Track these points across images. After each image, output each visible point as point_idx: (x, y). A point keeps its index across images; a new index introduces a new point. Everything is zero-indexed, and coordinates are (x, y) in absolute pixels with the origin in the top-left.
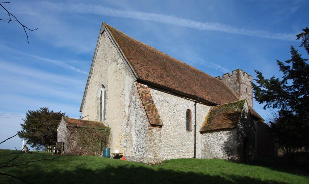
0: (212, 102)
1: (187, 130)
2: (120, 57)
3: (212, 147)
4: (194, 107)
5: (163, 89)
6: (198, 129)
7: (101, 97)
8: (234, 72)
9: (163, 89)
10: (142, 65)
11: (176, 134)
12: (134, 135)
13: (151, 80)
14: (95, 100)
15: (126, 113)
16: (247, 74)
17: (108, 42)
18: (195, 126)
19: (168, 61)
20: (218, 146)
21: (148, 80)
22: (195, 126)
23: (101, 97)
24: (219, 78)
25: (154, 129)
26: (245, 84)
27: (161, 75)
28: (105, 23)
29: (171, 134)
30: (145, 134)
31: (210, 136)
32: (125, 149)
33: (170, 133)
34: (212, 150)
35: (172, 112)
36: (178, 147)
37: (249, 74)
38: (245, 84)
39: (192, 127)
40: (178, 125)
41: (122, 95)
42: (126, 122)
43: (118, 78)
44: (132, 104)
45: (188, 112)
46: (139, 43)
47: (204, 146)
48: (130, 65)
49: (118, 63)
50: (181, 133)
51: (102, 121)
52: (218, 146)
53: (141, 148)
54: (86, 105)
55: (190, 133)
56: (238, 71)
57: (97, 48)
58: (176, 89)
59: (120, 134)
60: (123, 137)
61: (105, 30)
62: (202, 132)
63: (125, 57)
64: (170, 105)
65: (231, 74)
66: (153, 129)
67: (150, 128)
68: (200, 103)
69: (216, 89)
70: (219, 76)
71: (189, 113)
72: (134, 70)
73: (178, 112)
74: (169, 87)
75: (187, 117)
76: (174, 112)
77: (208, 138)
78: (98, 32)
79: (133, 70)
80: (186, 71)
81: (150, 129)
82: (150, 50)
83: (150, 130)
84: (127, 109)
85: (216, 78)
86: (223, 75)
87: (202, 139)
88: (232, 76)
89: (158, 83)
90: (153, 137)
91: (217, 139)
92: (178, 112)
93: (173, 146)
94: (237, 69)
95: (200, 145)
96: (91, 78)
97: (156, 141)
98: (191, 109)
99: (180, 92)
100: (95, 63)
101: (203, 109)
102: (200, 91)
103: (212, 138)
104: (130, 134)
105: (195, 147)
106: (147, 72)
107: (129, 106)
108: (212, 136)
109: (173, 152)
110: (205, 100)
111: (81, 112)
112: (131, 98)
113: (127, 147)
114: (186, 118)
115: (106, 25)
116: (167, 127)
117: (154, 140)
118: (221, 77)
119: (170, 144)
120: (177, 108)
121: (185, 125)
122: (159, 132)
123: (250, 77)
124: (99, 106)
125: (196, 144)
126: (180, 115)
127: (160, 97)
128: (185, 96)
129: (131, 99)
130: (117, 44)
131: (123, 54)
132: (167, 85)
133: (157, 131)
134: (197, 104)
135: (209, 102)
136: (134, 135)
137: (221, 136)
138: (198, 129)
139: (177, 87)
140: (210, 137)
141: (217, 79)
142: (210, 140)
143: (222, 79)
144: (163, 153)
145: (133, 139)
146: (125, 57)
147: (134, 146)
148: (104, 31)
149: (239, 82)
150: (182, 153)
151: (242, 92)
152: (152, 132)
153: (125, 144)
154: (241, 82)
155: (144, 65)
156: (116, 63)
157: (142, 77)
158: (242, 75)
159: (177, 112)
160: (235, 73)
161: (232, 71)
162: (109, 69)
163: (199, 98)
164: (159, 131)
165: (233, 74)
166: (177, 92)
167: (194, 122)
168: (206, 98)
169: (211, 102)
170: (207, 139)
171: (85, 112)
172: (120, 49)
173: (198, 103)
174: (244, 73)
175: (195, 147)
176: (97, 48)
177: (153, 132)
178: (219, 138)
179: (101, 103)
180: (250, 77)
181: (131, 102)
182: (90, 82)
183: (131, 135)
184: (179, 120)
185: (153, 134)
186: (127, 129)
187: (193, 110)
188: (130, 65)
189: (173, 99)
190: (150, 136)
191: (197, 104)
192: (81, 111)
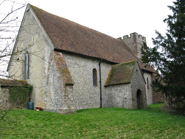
0: (113, 61)
18: (100, 81)
22: (100, 81)
25: (68, 88)
32: (46, 103)
39: (98, 83)
44: (51, 67)
45: (95, 70)
55: (97, 87)
64: (80, 66)
75: (93, 75)
84: (46, 71)
92: (86, 71)
97: (69, 96)
103: (113, 91)
107: (48, 69)
109: (83, 104)
120: (85, 69)
121: (92, 82)
137: (120, 89)
138: (103, 84)
150: (90, 104)
153: (46, 99)
164: (71, 88)
175: (101, 99)
178: (119, 91)
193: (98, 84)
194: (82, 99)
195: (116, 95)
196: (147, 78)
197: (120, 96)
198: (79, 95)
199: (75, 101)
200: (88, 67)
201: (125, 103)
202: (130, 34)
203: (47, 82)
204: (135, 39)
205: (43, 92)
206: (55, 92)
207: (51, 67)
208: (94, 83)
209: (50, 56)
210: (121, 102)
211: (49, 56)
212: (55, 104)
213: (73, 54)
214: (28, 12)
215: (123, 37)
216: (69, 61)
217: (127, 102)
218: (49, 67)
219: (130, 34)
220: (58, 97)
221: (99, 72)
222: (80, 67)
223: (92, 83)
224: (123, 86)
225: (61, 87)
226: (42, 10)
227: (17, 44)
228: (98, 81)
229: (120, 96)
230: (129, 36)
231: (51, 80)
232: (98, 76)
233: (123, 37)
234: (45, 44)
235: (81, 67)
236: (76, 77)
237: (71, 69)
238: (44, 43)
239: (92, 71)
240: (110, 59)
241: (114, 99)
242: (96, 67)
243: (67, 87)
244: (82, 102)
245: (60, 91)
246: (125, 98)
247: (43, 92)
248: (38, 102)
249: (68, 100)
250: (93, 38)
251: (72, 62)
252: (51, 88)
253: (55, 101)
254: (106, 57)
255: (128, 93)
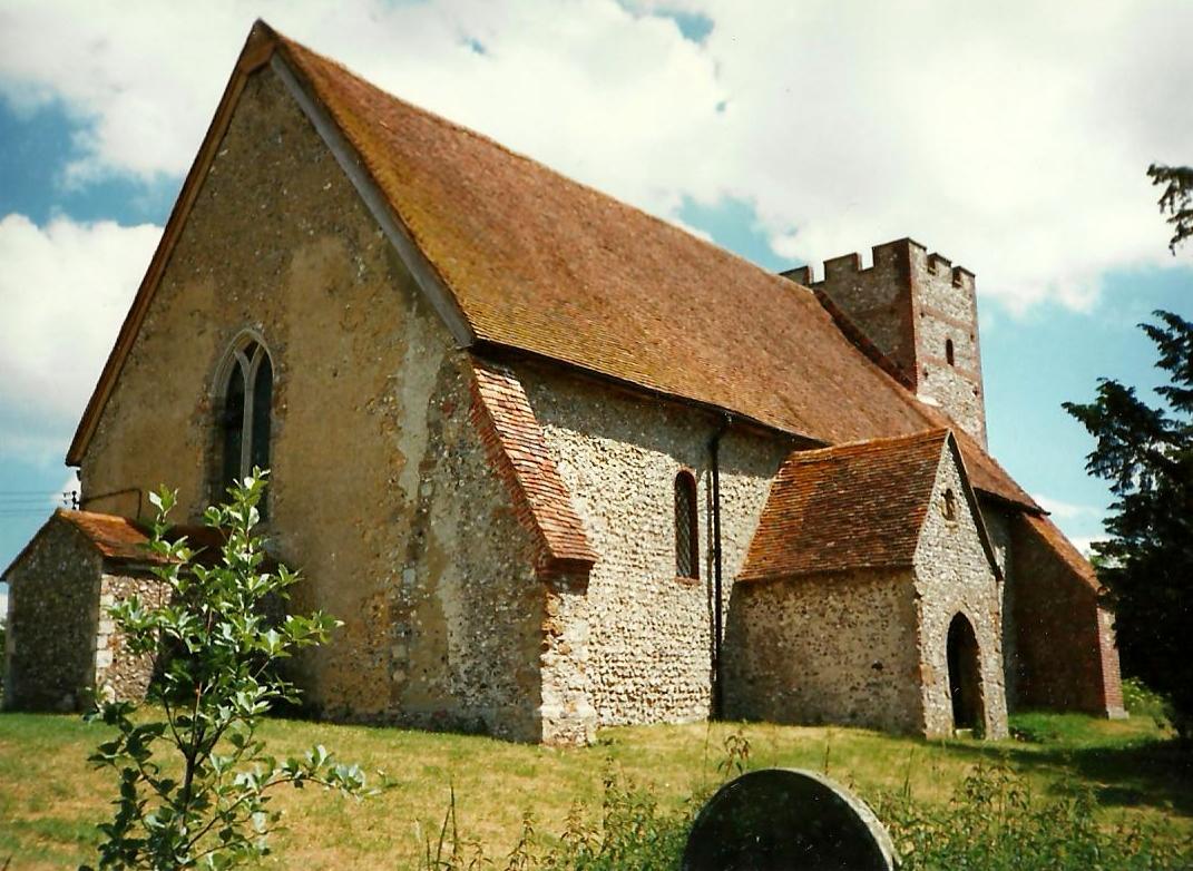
3: (800, 663)
26: (940, 316)
31: (786, 603)
32: (398, 676)
34: (803, 679)
37: (929, 252)
38: (940, 316)
47: (762, 658)
52: (828, 657)
53: (495, 670)
59: (364, 600)
64: (606, 455)
77: (781, 618)
82: (648, 217)
84: (410, 479)
107: (426, 466)
108: (800, 603)
112: (434, 427)
134: (723, 445)
137: (841, 606)
140: (791, 610)
142: (790, 625)
145: (450, 627)
147: (451, 662)
178: (834, 617)
180: (939, 265)
181: (435, 446)
183: (433, 602)
186: (410, 576)
195: (812, 640)
197: (839, 653)
201: (876, 693)
202: (876, 250)
205: (376, 608)
209: (442, 388)
210: (846, 688)
211: (434, 382)
212: (469, 684)
213: (636, 400)
215: (825, 263)
217: (889, 691)
218: (428, 453)
219: (876, 250)
220: (496, 640)
223: (668, 566)
224: (862, 590)
225: (523, 576)
226: (343, 72)
227: (165, 286)
229: (843, 647)
230: (867, 262)
231: (444, 530)
233: (825, 263)
234: (400, 309)
238: (391, 297)
241: (797, 668)
243: (558, 579)
244: (613, 679)
245: (515, 605)
247: (376, 608)
253: (469, 663)
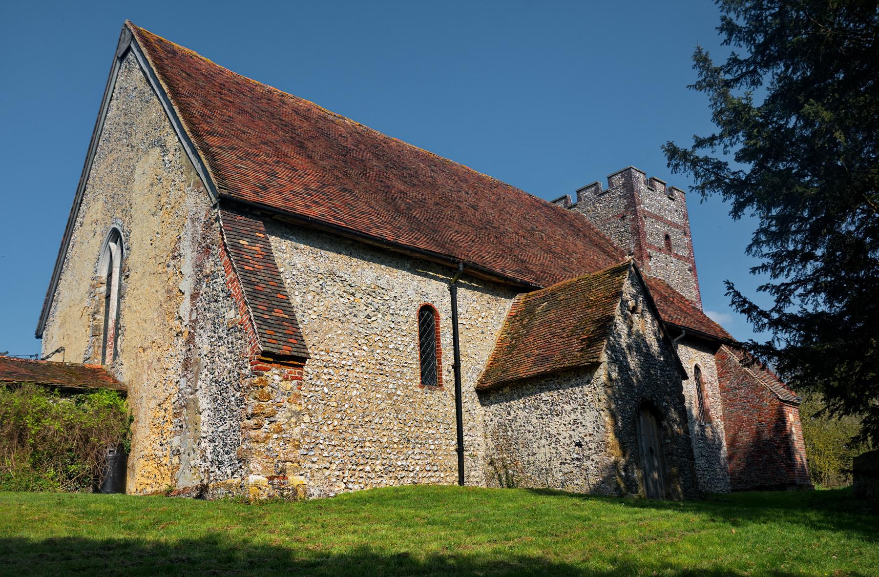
0: (519, 278)
1: (422, 383)
2: (171, 131)
4: (448, 298)
5: (322, 232)
6: (469, 383)
7: (110, 275)
8: (616, 178)
9: (322, 232)
10: (248, 154)
11: (379, 396)
12: (204, 403)
13: (274, 200)
14: (88, 287)
15: (185, 324)
16: (664, 184)
17: (138, 83)
18: (457, 367)
19: (362, 146)
20: (543, 441)
21: (260, 199)
22: (457, 367)
23: (110, 275)
24: (566, 203)
25: (274, 374)
26: (659, 219)
27: (321, 188)
28: (132, 24)
29: (360, 396)
30: (238, 394)
32: (176, 460)
33: (355, 393)
35: (362, 316)
36: (389, 451)
38: (659, 219)
39: (445, 372)
40: (385, 362)
41: (174, 257)
42: (181, 357)
43: (164, 200)
44: (204, 286)
45: (427, 314)
46: (258, 88)
48: (201, 153)
49: (165, 151)
50: (399, 392)
51: (108, 360)
54: (59, 311)
55: (438, 393)
56: (627, 173)
57: (106, 107)
58: (374, 232)
59: (159, 405)
60: (169, 417)
61: (133, 46)
62: (485, 394)
63: (186, 129)
64: (352, 290)
65: (604, 186)
66: (268, 370)
67: (257, 369)
68: (468, 287)
69: (546, 238)
70: (563, 195)
71: (431, 321)
72: (211, 167)
73: (384, 315)
74: (344, 225)
75: (421, 337)
76: (368, 316)
78: (111, 52)
79: (209, 169)
80: (432, 177)
81: (256, 373)
83: (256, 374)
84: (186, 305)
85: (555, 202)
86: (578, 192)
87: (487, 418)
88: (607, 192)
89: (300, 209)
90: (270, 402)
91: (539, 412)
92: (384, 315)
93: (367, 444)
94: (622, 169)
95: (480, 440)
96: (81, 211)
97: (281, 417)
98: (435, 305)
99: (388, 243)
100: (97, 156)
101: (485, 303)
102: (473, 241)
103: (520, 412)
104: (193, 400)
105: (460, 450)
106: (263, 177)
107: (194, 296)
109: (368, 468)
110: (492, 273)
111: (41, 337)
112: (199, 267)
113: (182, 451)
114: (417, 338)
115: (135, 28)
116: (342, 372)
117: (275, 413)
118: (573, 200)
119: (356, 438)
120: (378, 302)
121: (416, 365)
122: (295, 382)
123: (676, 193)
124: (102, 309)
125: (465, 438)
126: (393, 325)
127: (310, 262)
128: (408, 258)
129: (201, 271)
130: (165, 87)
131: (181, 119)
132: (334, 217)
133: (286, 379)
134: (461, 291)
135: (506, 278)
136: (204, 403)
138: (469, 383)
139: (378, 227)
141: (560, 205)
143: (575, 205)
144: (327, 473)
146: (186, 129)
148: (129, 49)
149: (635, 212)
150: (404, 474)
151: (650, 246)
152: (263, 384)
153: (176, 441)
154: (644, 211)
155: (259, 155)
156: (158, 149)
157: (240, 189)
158: (643, 187)
159: (380, 316)
160: (619, 181)
161: (609, 175)
162: (138, 171)
163: (465, 265)
164: (293, 378)
165: (611, 184)
166: (376, 244)
167: (452, 352)
168: (494, 264)
169: (513, 280)
170: (504, 414)
171: (54, 335)
172: (172, 101)
173: (462, 286)
174: (651, 183)
175: (460, 450)
176: (106, 107)
177: (270, 381)
179: (108, 297)
180: (676, 193)
182: (78, 224)
184: (391, 346)
185: (268, 389)
187: (443, 307)
188: (201, 153)
189: (363, 269)
190: (256, 398)
191: (461, 291)
192: (39, 336)
193: (447, 376)
194: (361, 443)
196: (697, 368)
198: (345, 423)
199: (325, 454)
200: (393, 294)
203: (187, 360)
204: (633, 196)
206: (215, 400)
207: (204, 286)
208: (422, 374)
214: (124, 63)
216: (299, 260)
217: (588, 463)
221: (450, 322)
222: (353, 294)
225: (243, 372)
228: (447, 361)
229: (553, 432)
232: (446, 339)
235: (358, 295)
236: (331, 339)
237: (310, 297)
239: (414, 316)
240: (508, 269)
242: (435, 299)
246: (579, 445)
248: (142, 461)
249: (275, 436)
250: (433, 185)
251: (312, 268)
252: (200, 383)
254: (488, 258)
255: (590, 416)
